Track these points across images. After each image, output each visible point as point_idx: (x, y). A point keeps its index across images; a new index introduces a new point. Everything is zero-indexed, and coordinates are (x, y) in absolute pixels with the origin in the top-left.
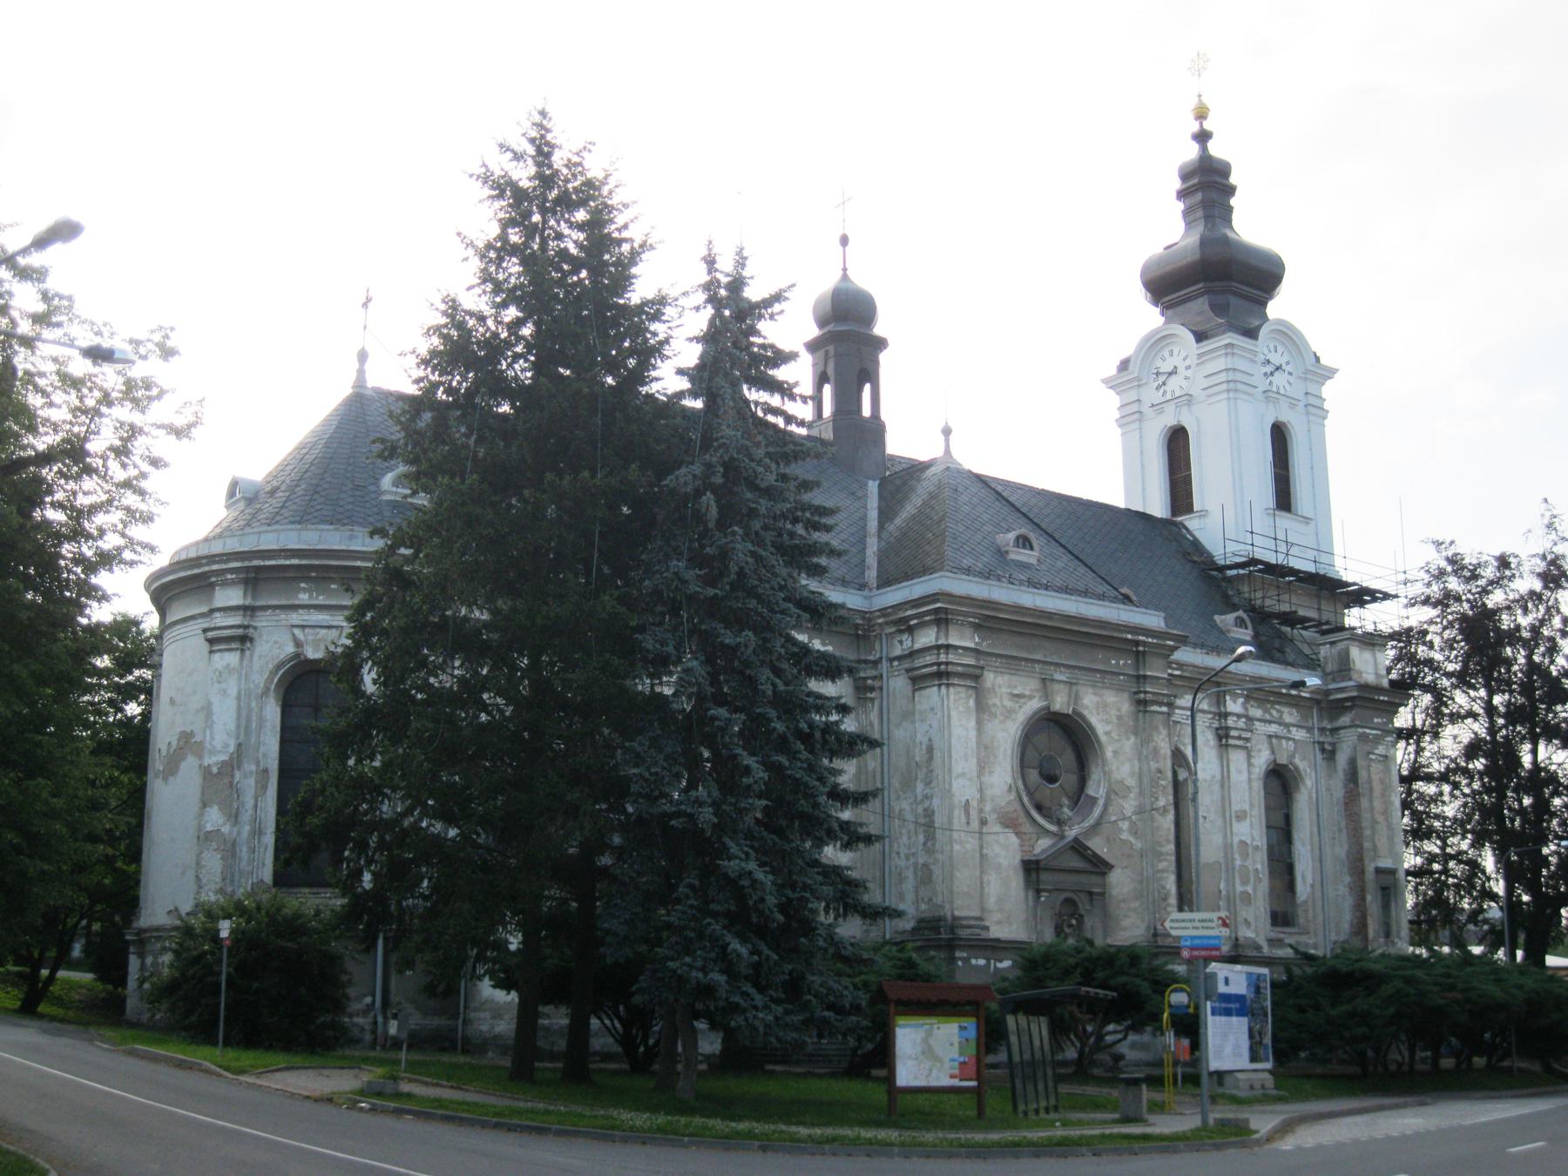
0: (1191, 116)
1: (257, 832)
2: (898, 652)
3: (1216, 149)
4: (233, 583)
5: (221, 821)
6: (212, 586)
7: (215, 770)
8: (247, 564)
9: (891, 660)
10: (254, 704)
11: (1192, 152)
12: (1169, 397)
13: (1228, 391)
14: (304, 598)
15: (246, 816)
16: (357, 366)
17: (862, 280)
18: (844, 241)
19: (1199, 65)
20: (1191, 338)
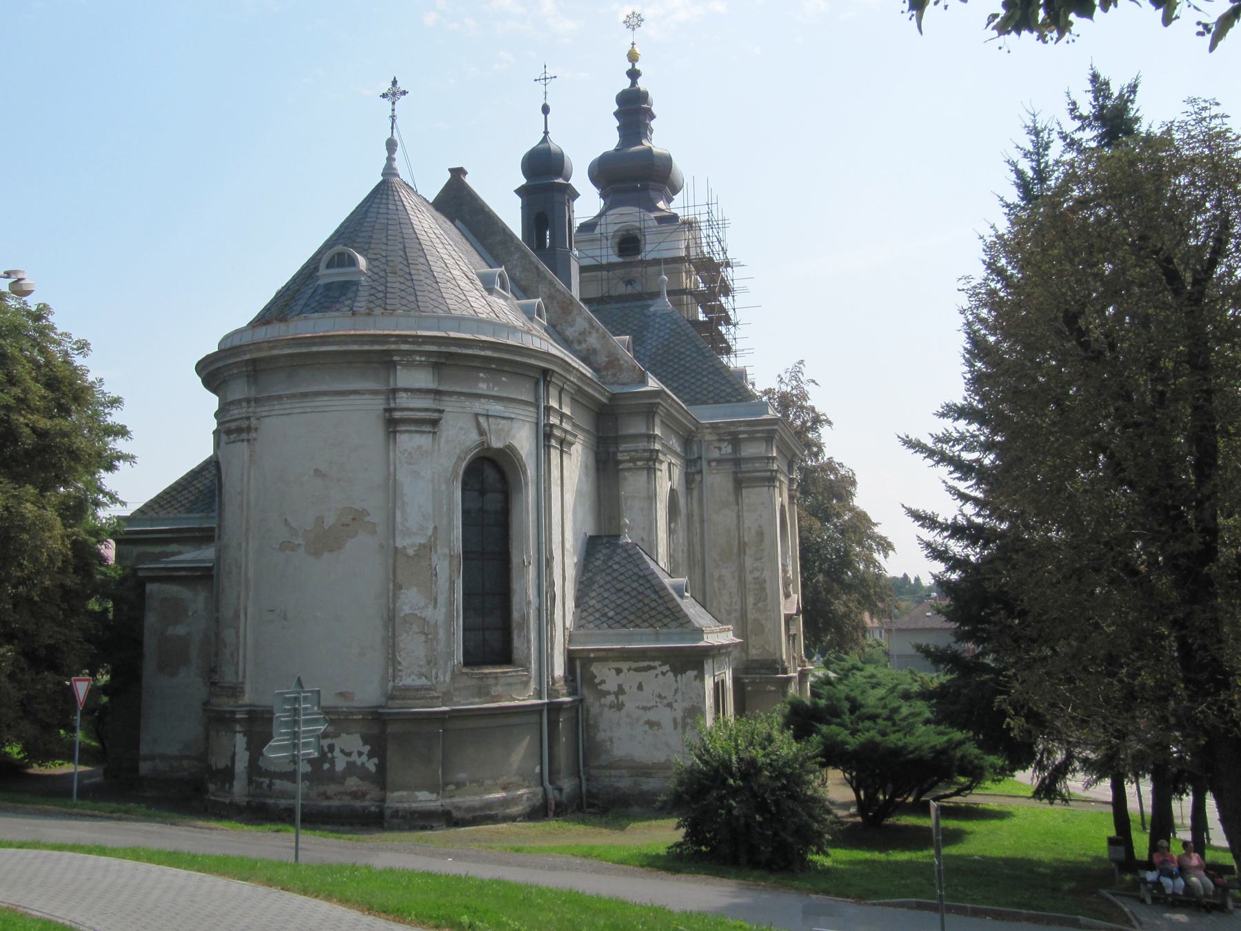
1: (450, 617)
2: (716, 454)
3: (642, 84)
4: (421, 365)
7: (411, 552)
8: (443, 349)
11: (626, 83)
14: (483, 387)
15: (442, 599)
16: (396, 156)
17: (558, 141)
18: (546, 110)
19: (634, 22)
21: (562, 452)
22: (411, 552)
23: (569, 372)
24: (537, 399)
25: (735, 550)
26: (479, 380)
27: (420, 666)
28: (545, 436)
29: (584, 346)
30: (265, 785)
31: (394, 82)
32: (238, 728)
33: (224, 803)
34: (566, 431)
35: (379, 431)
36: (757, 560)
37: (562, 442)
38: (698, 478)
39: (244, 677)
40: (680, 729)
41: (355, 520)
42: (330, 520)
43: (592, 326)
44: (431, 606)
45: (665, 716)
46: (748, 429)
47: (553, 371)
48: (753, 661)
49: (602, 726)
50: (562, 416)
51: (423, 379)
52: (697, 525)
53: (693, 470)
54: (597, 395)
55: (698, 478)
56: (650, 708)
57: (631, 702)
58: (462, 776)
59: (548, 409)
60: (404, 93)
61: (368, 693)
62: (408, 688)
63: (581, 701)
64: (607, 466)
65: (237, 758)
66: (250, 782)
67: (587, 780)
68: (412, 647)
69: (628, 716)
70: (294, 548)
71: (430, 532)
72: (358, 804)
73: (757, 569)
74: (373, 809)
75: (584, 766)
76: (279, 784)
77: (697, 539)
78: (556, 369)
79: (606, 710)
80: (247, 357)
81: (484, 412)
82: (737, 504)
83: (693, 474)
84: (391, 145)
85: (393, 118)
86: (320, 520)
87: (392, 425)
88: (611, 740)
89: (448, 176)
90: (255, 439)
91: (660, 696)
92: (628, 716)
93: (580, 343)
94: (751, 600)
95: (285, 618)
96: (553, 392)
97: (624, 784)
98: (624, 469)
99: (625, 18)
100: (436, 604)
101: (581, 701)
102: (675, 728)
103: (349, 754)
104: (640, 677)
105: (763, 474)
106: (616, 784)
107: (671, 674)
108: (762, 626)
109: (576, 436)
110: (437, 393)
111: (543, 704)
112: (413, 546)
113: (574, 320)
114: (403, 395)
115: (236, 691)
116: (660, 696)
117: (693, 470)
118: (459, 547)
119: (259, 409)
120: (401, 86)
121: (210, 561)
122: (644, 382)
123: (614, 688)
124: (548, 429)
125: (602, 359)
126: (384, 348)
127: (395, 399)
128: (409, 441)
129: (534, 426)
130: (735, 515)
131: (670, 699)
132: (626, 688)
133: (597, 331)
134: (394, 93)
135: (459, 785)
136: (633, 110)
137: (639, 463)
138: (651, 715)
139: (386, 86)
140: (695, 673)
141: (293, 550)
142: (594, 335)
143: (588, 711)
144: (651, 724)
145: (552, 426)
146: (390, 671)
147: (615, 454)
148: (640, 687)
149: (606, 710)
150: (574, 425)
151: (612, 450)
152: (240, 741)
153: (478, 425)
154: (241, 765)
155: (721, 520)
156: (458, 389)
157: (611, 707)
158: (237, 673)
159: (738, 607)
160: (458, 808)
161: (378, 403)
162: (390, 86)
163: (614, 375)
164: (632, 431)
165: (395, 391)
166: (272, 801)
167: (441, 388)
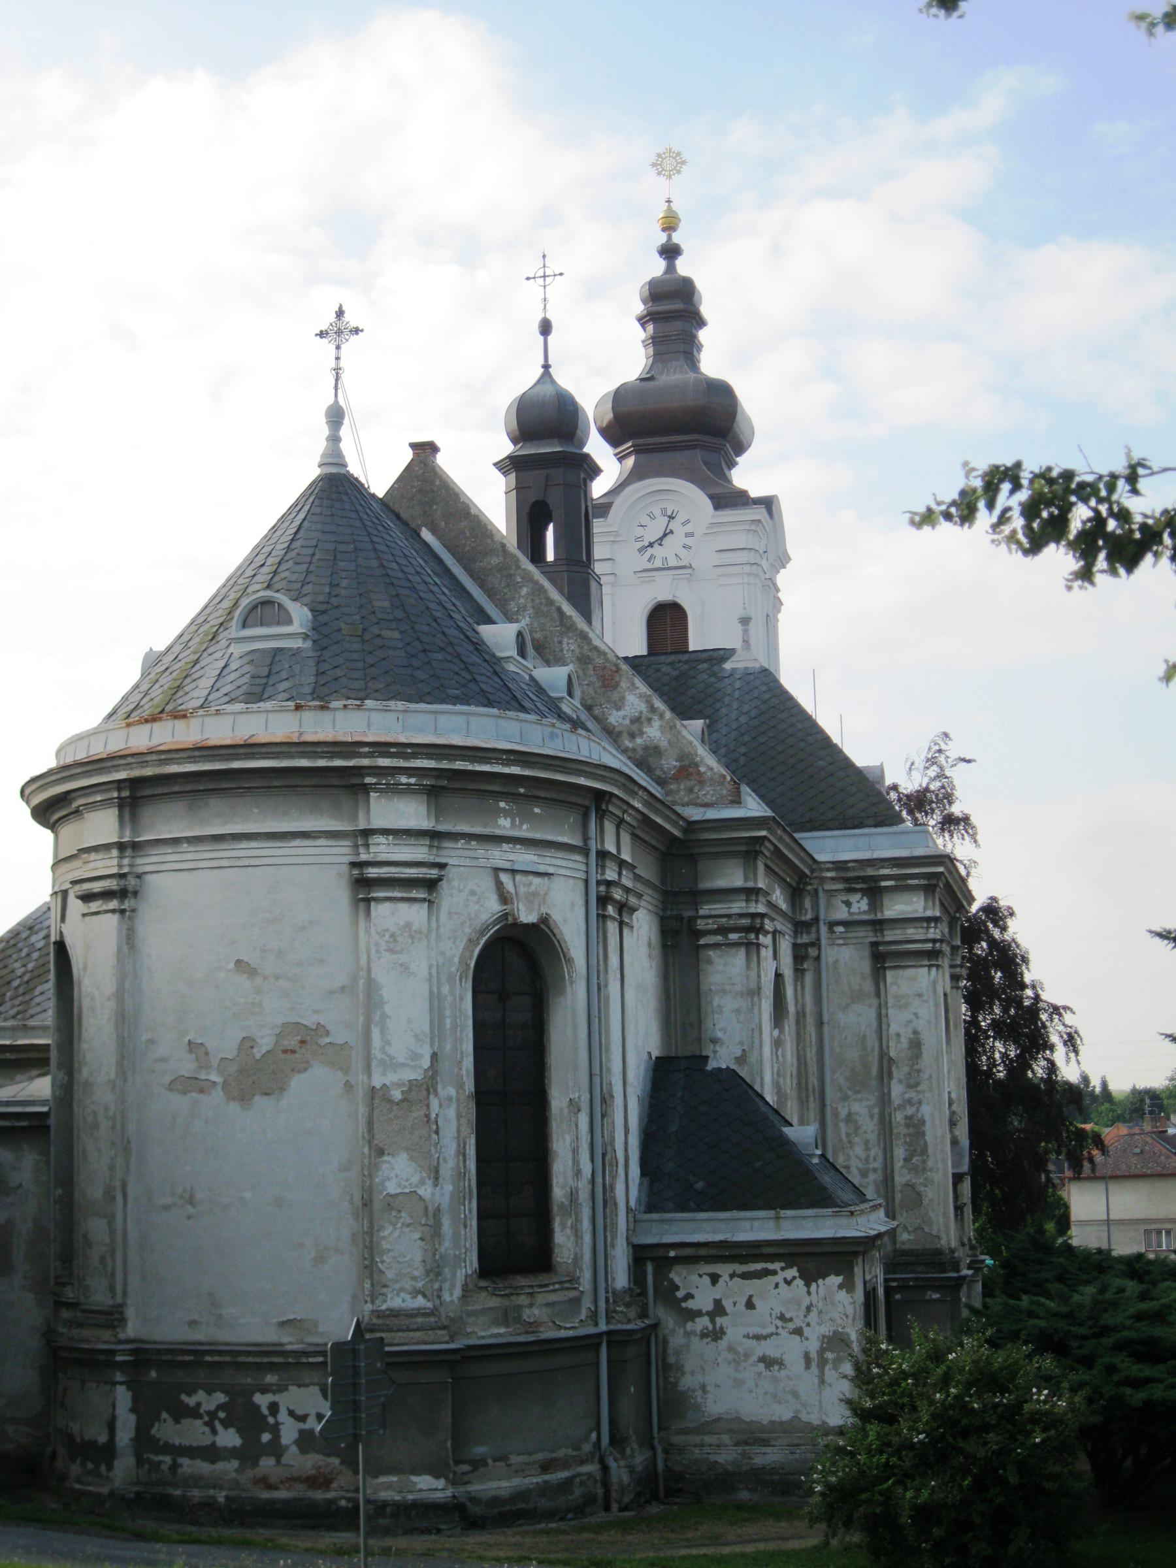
0: (657, 227)
2: (841, 913)
3: (683, 267)
4: (408, 790)
5: (415, 1179)
6: (366, 789)
7: (397, 1095)
8: (445, 765)
9: (832, 925)
10: (446, 989)
11: (658, 267)
12: (658, 563)
13: (749, 574)
14: (504, 825)
15: (447, 1170)
16: (325, 431)
17: (566, 380)
20: (707, 504)
21: (621, 924)
22: (397, 1095)
23: (633, 794)
24: (586, 839)
25: (874, 1071)
26: (499, 812)
27: (414, 1278)
28: (606, 905)
29: (639, 741)
30: (164, 1467)
31: (340, 313)
32: (119, 1377)
33: (98, 1496)
34: (627, 890)
35: (342, 894)
36: (910, 1086)
37: (622, 907)
38: (812, 952)
39: (125, 1294)
40: (814, 1369)
41: (302, 1044)
42: (265, 1043)
43: (652, 709)
44: (429, 1183)
45: (790, 1349)
46: (895, 871)
47: (611, 794)
48: (905, 1253)
49: (689, 1365)
50: (622, 864)
51: (412, 813)
52: (811, 1029)
53: (805, 939)
54: (667, 826)
55: (812, 952)
56: (765, 1337)
57: (736, 1329)
58: (481, 1450)
59: (603, 855)
60: (357, 331)
61: (338, 1326)
62: (395, 1313)
63: (655, 1326)
64: (681, 944)
65: (119, 1424)
66: (140, 1461)
67: (666, 1451)
68: (403, 1248)
69: (731, 1349)
70: (203, 1088)
71: (426, 1063)
72: (319, 1495)
73: (909, 1102)
74: (343, 1503)
75: (660, 1429)
76: (188, 1466)
77: (811, 1055)
78: (616, 791)
79: (695, 1340)
80: (122, 775)
81: (507, 865)
82: (878, 995)
83: (806, 945)
84: (336, 417)
85: (337, 370)
86: (248, 1043)
87: (365, 886)
88: (703, 1387)
89: (408, 455)
90: (133, 911)
91: (782, 1317)
92: (731, 1349)
93: (632, 736)
94: (900, 1153)
95: (191, 1201)
96: (609, 827)
97: (726, 1456)
98: (707, 946)
99: (685, 169)
100: (437, 1179)
101: (655, 1326)
102: (808, 1365)
103: (303, 1418)
104: (751, 1286)
105: (919, 946)
106: (712, 1458)
107: (799, 1282)
108: (919, 1194)
109: (640, 896)
110: (434, 837)
111: (601, 1335)
112: (399, 1084)
113: (622, 699)
114: (381, 839)
115: (113, 1317)
116: (782, 1317)
117: (805, 939)
118: (470, 1086)
119: (139, 861)
120: (351, 319)
121: (44, 1103)
122: (737, 801)
123: (710, 1307)
124: (602, 888)
125: (670, 763)
126: (351, 763)
127: (367, 846)
128: (390, 914)
129: (581, 886)
130: (873, 1015)
131: (798, 1323)
132: (727, 1304)
133: (661, 716)
134: (339, 330)
135: (478, 1464)
136: (673, 312)
137: (734, 936)
138: (768, 1348)
139: (327, 319)
140: (839, 1279)
141: (202, 1091)
142: (657, 724)
143: (665, 1342)
144: (768, 1362)
145: (609, 884)
146: (367, 1286)
147: (693, 919)
148: (750, 1305)
149: (695, 1340)
150: (637, 878)
151: (687, 914)
152: (123, 1397)
153: (499, 885)
154: (125, 1435)
155: (852, 1020)
156: (466, 829)
157: (703, 1335)
158: (112, 1288)
159: (878, 1164)
160: (474, 1500)
161: (341, 852)
162: (332, 317)
163: (690, 790)
164: (721, 883)
165: (367, 833)
166: (178, 1492)
167: (440, 828)
